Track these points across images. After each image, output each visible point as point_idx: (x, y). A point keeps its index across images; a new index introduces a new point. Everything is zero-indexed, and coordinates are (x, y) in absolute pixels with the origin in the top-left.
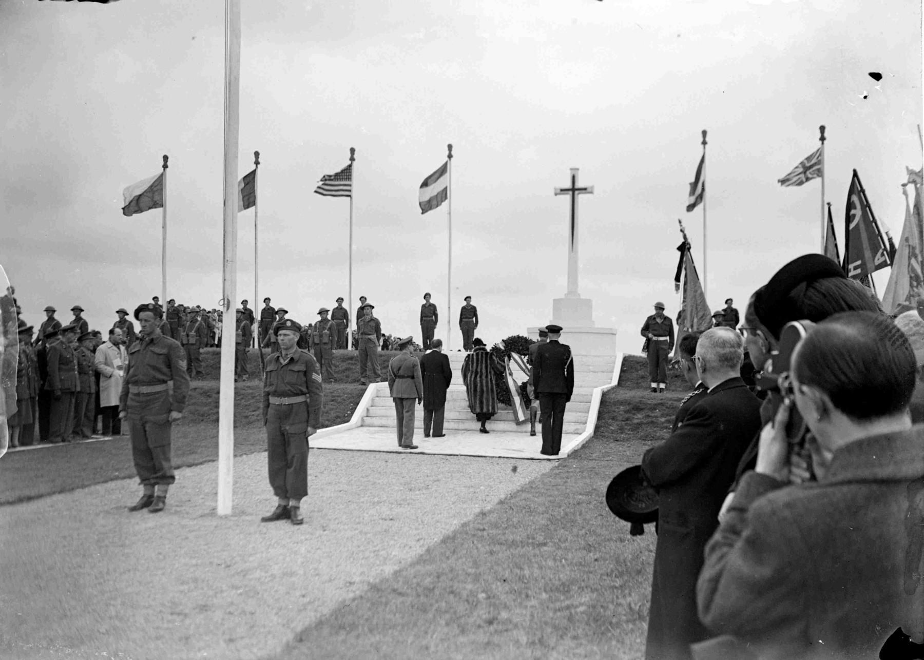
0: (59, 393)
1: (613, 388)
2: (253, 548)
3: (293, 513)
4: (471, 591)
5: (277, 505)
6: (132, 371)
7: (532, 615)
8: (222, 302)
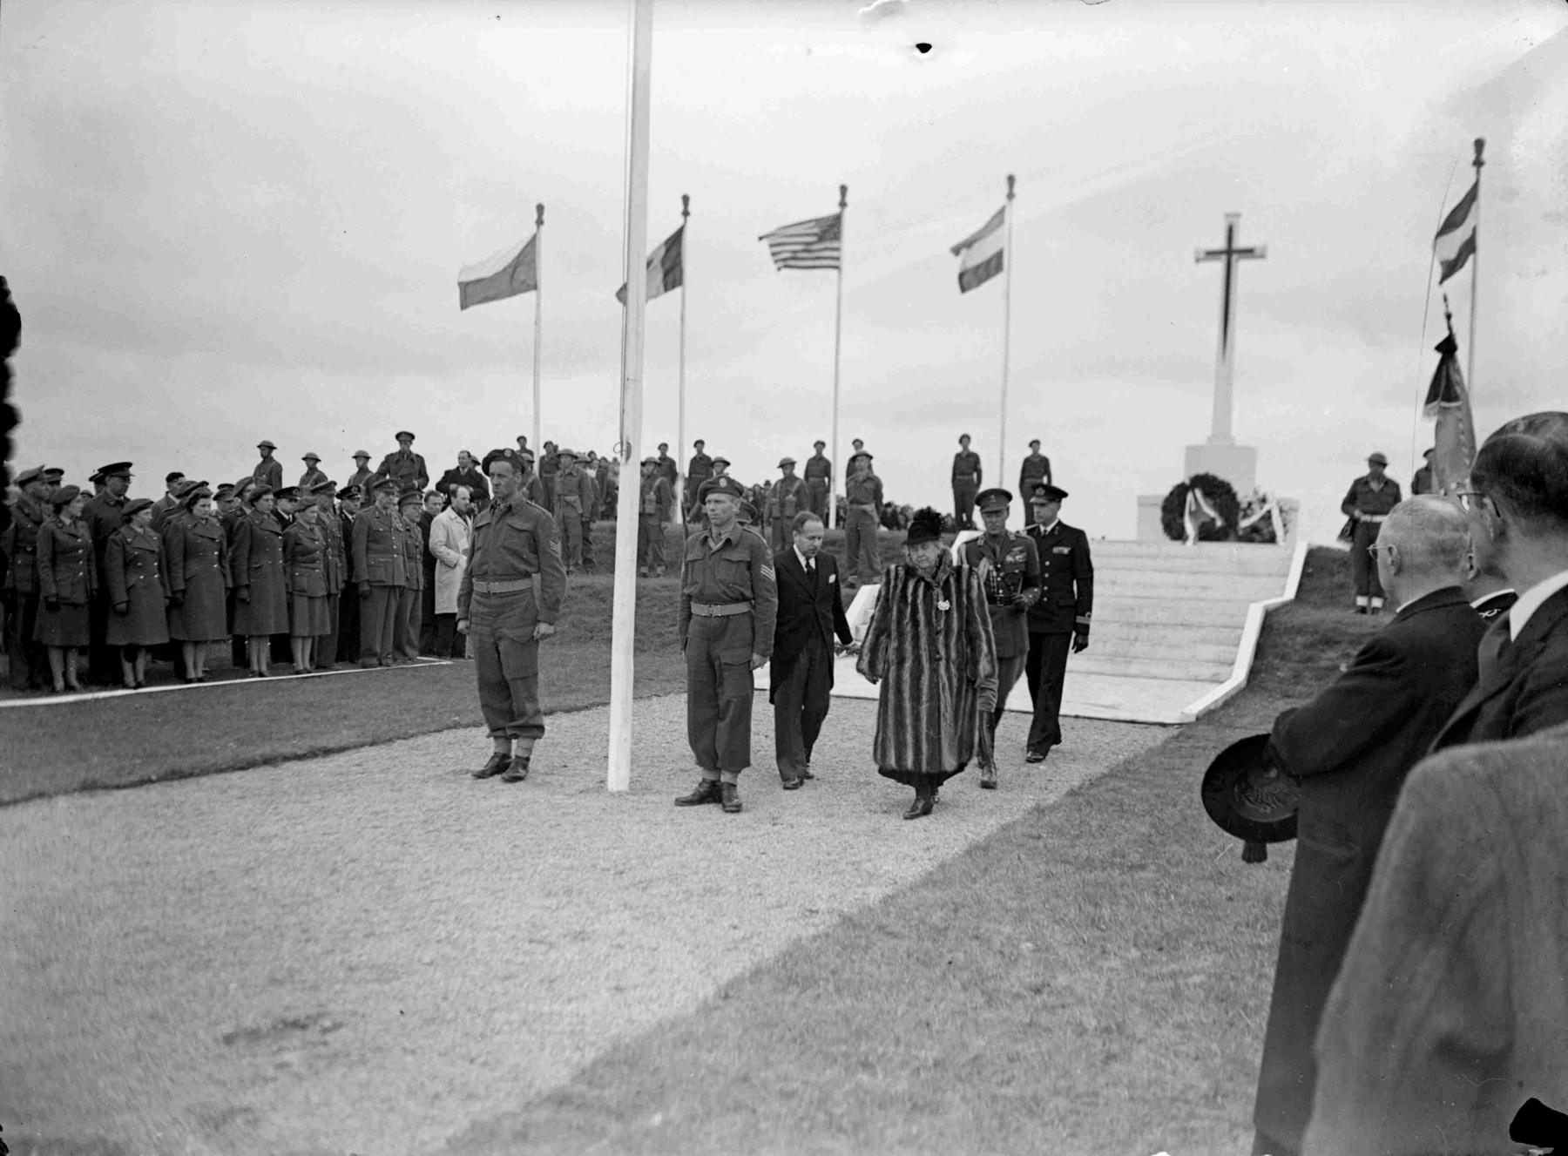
0: (366, 588)
1: (1285, 605)
2: (661, 846)
3: (725, 793)
4: (1009, 938)
5: (700, 779)
6: (478, 555)
7: (1109, 984)
8: (618, 448)
